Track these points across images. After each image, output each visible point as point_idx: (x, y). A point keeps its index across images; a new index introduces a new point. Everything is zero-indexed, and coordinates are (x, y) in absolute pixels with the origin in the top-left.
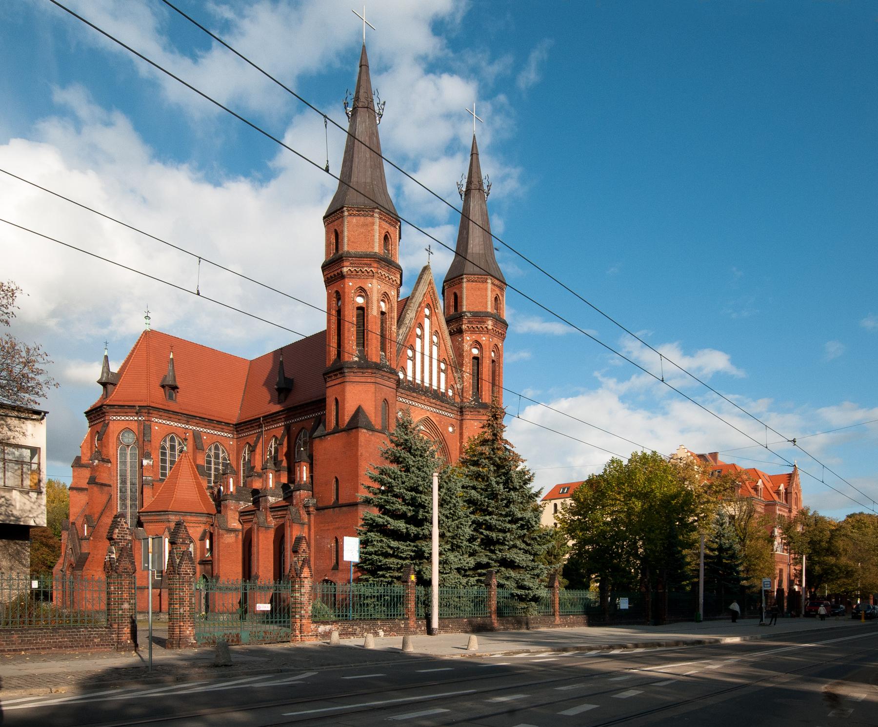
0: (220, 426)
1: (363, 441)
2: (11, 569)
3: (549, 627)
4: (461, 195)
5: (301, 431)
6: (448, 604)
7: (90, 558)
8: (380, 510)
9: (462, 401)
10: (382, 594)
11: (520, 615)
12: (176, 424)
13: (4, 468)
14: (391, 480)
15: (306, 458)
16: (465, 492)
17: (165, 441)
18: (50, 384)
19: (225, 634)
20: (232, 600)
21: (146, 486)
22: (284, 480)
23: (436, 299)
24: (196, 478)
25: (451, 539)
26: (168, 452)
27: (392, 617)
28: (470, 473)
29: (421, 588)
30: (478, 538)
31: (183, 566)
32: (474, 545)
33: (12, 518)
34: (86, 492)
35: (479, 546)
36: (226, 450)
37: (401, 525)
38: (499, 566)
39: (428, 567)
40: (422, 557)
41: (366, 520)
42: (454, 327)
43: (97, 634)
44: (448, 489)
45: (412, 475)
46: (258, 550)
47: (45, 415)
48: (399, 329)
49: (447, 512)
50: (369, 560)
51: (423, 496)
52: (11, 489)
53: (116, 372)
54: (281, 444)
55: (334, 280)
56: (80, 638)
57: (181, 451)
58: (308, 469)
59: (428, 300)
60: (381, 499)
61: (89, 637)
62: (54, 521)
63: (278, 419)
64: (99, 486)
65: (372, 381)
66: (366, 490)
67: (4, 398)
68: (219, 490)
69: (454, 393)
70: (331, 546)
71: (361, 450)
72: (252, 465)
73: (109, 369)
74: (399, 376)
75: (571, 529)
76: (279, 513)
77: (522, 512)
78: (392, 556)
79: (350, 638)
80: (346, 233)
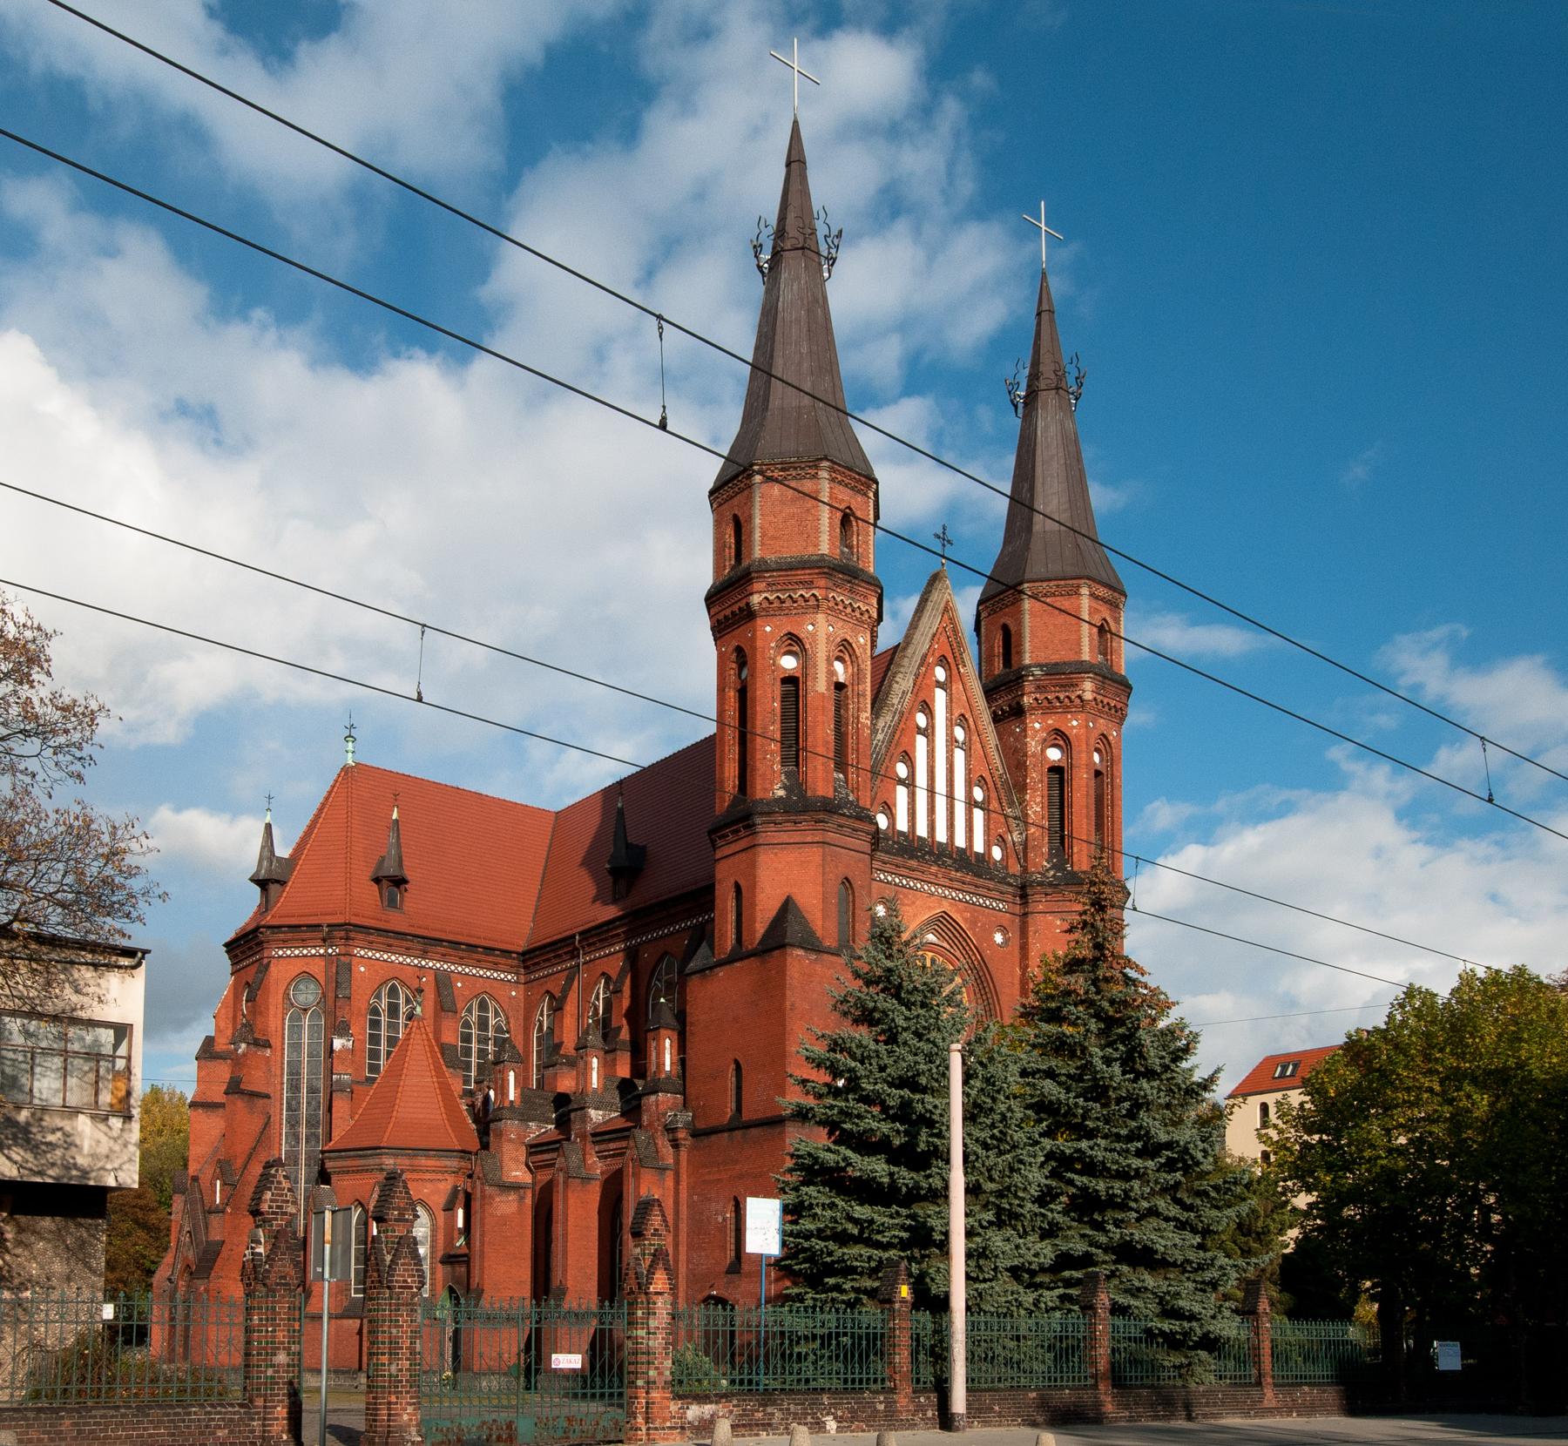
0: (491, 959)
1: (796, 975)
2: (69, 1279)
3: (1247, 1415)
4: (1016, 407)
5: (660, 960)
6: (990, 1354)
7: (224, 1253)
8: (830, 1134)
9: (1025, 870)
10: (834, 1330)
11: (1171, 1383)
12: (401, 959)
13: (65, 1069)
14: (853, 1064)
15: (673, 1022)
16: (1028, 1084)
17: (378, 997)
18: (151, 894)
19: (484, 1423)
20: (506, 1345)
21: (339, 1094)
22: (624, 1071)
23: (960, 644)
24: (439, 1074)
25: (997, 1197)
26: (384, 1019)
27: (857, 1386)
28: (1040, 1041)
29: (925, 1317)
30: (1062, 1194)
31: (400, 1270)
32: (1052, 1211)
33: (74, 1173)
34: (221, 1110)
35: (1065, 1212)
36: (503, 1010)
37: (878, 1167)
38: (1115, 1262)
39: (942, 1266)
40: (927, 1241)
41: (799, 1157)
42: (1003, 702)
43: (223, 1419)
44: (987, 1080)
45: (902, 1051)
46: (565, 1229)
47: (143, 958)
48: (877, 718)
49: (984, 1135)
50: (805, 1250)
51: (928, 1098)
52: (75, 1112)
53: (287, 856)
54: (617, 991)
55: (733, 624)
56: (188, 1427)
57: (410, 1017)
58: (676, 1045)
59: (942, 647)
60: (831, 1107)
61: (207, 1427)
62: (161, 1175)
63: (612, 937)
64: (246, 1098)
65: (817, 839)
66: (798, 1088)
67: (67, 930)
68: (487, 1098)
69: (1005, 857)
70: (725, 1219)
71: (793, 997)
72: (556, 1041)
73: (272, 852)
74: (876, 824)
75: (1302, 1169)
76: (612, 1146)
77: (1170, 1129)
78: (857, 1240)
79: (757, 1435)
80: (757, 521)
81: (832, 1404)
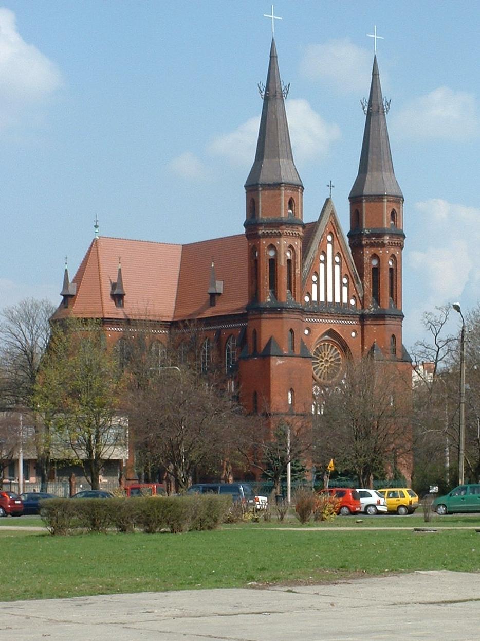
5: (230, 336)
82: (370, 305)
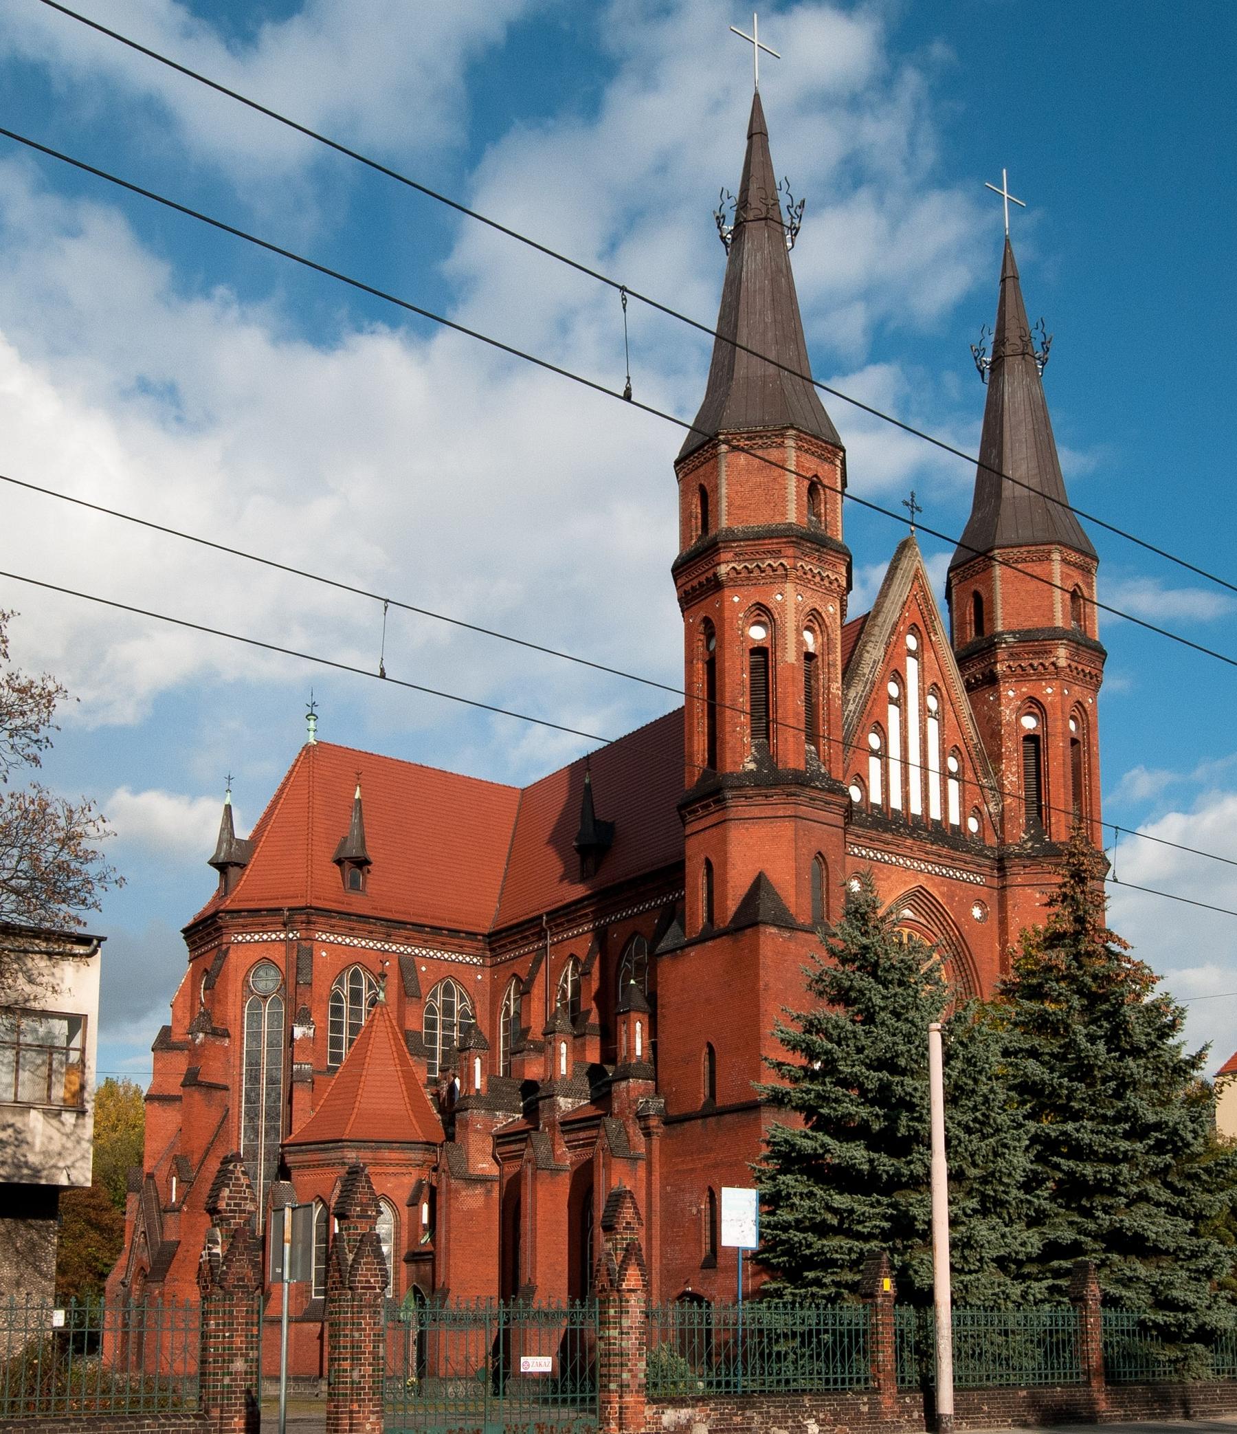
81: (813, 1406)
82: (1023, 835)
